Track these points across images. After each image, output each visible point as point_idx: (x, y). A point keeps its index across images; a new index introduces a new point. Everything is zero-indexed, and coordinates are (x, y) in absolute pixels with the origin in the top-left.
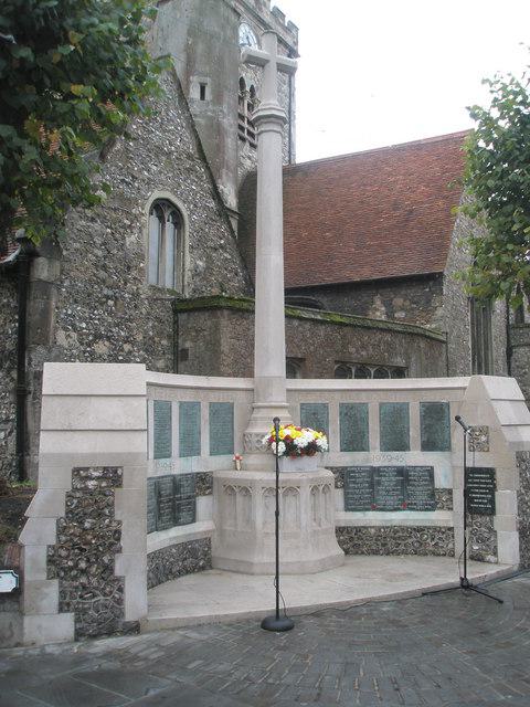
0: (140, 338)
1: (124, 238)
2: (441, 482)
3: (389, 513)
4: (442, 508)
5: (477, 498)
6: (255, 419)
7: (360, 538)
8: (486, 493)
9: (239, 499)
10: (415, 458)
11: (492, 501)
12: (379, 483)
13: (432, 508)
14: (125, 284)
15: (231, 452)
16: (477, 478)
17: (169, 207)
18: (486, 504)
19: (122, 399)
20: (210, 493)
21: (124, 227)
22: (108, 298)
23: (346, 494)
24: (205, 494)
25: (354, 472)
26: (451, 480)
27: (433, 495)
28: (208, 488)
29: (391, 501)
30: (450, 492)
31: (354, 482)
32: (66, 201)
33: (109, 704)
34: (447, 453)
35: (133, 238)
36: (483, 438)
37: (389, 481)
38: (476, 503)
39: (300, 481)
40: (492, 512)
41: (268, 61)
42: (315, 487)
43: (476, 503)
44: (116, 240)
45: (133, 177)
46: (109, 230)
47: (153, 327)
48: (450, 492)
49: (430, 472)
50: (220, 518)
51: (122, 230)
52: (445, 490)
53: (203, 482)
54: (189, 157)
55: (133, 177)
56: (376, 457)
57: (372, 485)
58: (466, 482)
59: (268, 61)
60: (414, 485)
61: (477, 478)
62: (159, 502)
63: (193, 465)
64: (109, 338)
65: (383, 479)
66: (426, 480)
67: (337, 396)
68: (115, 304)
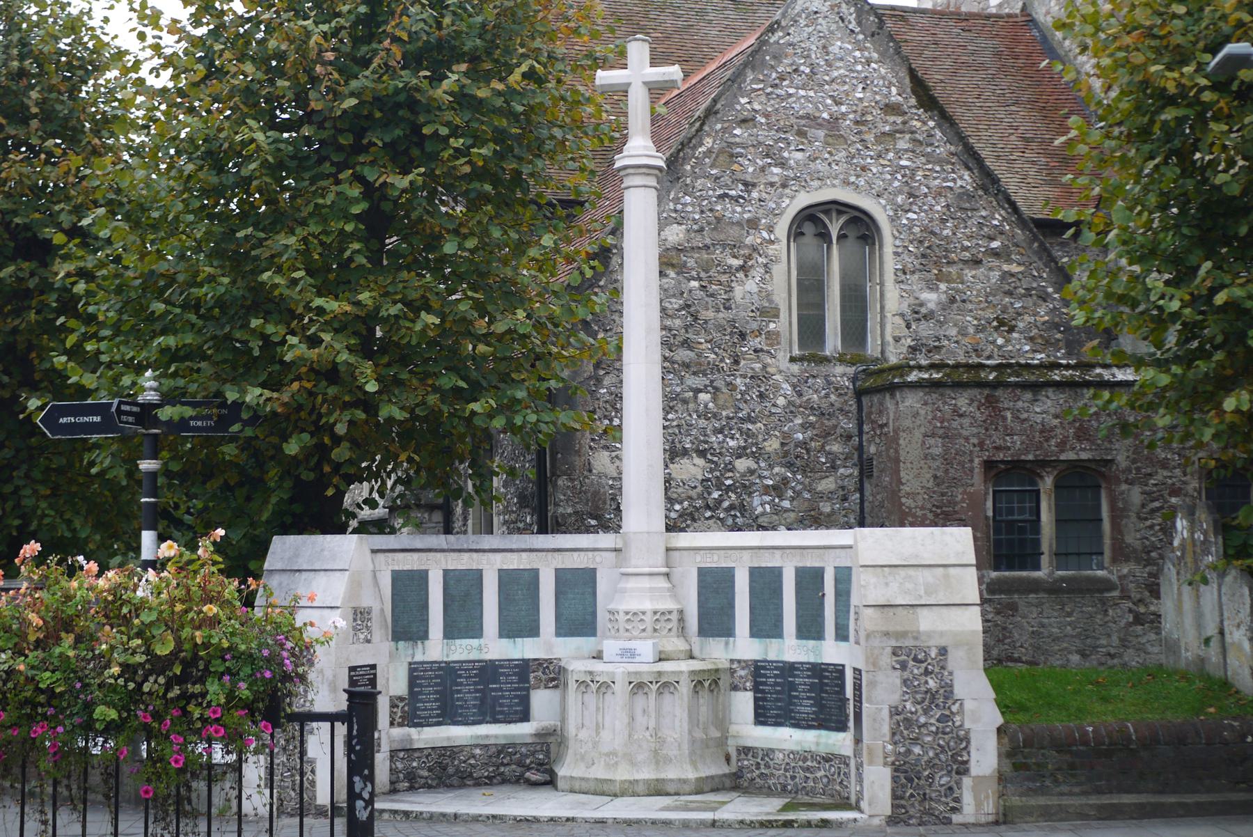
0: (772, 445)
1: (731, 289)
6: (624, 591)
7: (767, 766)
14: (736, 362)
17: (840, 213)
19: (540, 554)
20: (556, 687)
21: (730, 271)
22: (697, 391)
28: (553, 679)
35: (751, 285)
41: (629, 84)
42: (699, 682)
44: (712, 295)
45: (746, 184)
46: (695, 284)
47: (805, 427)
51: (724, 278)
54: (891, 109)
55: (746, 184)
58: (375, 675)
59: (629, 84)
63: (526, 649)
64: (702, 454)
67: (746, 555)
68: (714, 399)
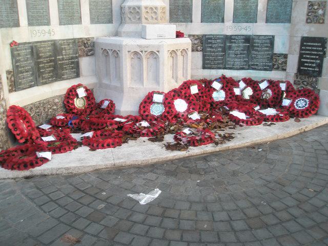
2: (279, 48)
3: (236, 71)
4: (278, 69)
5: (307, 62)
8: (316, 59)
9: (112, 59)
10: (261, 29)
11: (320, 66)
12: (230, 48)
13: (271, 68)
15: (110, 21)
16: (310, 46)
18: (314, 67)
20: (92, 55)
23: (204, 56)
24: (87, 55)
25: (211, 39)
26: (288, 48)
27: (272, 58)
28: (91, 50)
29: (238, 62)
30: (285, 56)
31: (211, 47)
32: (53, 152)
33: (14, 245)
34: (287, 25)
36: (320, 12)
37: (238, 47)
38: (306, 66)
39: (159, 46)
40: (320, 73)
43: (306, 66)
48: (285, 56)
49: (271, 40)
50: (96, 73)
52: (280, 55)
53: (88, 47)
56: (228, 28)
57: (224, 50)
58: (301, 49)
60: (257, 51)
61: (310, 46)
62: (38, 64)
65: (233, 45)
66: (267, 47)
